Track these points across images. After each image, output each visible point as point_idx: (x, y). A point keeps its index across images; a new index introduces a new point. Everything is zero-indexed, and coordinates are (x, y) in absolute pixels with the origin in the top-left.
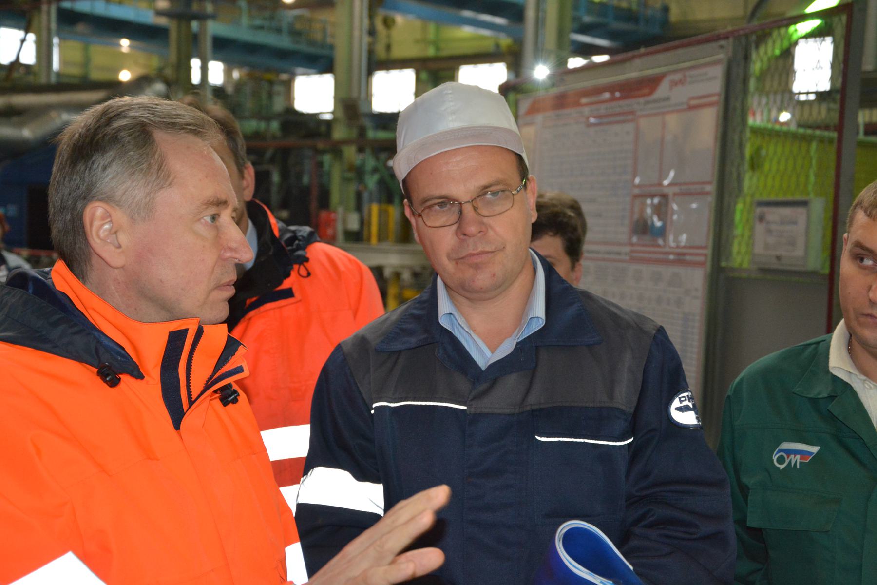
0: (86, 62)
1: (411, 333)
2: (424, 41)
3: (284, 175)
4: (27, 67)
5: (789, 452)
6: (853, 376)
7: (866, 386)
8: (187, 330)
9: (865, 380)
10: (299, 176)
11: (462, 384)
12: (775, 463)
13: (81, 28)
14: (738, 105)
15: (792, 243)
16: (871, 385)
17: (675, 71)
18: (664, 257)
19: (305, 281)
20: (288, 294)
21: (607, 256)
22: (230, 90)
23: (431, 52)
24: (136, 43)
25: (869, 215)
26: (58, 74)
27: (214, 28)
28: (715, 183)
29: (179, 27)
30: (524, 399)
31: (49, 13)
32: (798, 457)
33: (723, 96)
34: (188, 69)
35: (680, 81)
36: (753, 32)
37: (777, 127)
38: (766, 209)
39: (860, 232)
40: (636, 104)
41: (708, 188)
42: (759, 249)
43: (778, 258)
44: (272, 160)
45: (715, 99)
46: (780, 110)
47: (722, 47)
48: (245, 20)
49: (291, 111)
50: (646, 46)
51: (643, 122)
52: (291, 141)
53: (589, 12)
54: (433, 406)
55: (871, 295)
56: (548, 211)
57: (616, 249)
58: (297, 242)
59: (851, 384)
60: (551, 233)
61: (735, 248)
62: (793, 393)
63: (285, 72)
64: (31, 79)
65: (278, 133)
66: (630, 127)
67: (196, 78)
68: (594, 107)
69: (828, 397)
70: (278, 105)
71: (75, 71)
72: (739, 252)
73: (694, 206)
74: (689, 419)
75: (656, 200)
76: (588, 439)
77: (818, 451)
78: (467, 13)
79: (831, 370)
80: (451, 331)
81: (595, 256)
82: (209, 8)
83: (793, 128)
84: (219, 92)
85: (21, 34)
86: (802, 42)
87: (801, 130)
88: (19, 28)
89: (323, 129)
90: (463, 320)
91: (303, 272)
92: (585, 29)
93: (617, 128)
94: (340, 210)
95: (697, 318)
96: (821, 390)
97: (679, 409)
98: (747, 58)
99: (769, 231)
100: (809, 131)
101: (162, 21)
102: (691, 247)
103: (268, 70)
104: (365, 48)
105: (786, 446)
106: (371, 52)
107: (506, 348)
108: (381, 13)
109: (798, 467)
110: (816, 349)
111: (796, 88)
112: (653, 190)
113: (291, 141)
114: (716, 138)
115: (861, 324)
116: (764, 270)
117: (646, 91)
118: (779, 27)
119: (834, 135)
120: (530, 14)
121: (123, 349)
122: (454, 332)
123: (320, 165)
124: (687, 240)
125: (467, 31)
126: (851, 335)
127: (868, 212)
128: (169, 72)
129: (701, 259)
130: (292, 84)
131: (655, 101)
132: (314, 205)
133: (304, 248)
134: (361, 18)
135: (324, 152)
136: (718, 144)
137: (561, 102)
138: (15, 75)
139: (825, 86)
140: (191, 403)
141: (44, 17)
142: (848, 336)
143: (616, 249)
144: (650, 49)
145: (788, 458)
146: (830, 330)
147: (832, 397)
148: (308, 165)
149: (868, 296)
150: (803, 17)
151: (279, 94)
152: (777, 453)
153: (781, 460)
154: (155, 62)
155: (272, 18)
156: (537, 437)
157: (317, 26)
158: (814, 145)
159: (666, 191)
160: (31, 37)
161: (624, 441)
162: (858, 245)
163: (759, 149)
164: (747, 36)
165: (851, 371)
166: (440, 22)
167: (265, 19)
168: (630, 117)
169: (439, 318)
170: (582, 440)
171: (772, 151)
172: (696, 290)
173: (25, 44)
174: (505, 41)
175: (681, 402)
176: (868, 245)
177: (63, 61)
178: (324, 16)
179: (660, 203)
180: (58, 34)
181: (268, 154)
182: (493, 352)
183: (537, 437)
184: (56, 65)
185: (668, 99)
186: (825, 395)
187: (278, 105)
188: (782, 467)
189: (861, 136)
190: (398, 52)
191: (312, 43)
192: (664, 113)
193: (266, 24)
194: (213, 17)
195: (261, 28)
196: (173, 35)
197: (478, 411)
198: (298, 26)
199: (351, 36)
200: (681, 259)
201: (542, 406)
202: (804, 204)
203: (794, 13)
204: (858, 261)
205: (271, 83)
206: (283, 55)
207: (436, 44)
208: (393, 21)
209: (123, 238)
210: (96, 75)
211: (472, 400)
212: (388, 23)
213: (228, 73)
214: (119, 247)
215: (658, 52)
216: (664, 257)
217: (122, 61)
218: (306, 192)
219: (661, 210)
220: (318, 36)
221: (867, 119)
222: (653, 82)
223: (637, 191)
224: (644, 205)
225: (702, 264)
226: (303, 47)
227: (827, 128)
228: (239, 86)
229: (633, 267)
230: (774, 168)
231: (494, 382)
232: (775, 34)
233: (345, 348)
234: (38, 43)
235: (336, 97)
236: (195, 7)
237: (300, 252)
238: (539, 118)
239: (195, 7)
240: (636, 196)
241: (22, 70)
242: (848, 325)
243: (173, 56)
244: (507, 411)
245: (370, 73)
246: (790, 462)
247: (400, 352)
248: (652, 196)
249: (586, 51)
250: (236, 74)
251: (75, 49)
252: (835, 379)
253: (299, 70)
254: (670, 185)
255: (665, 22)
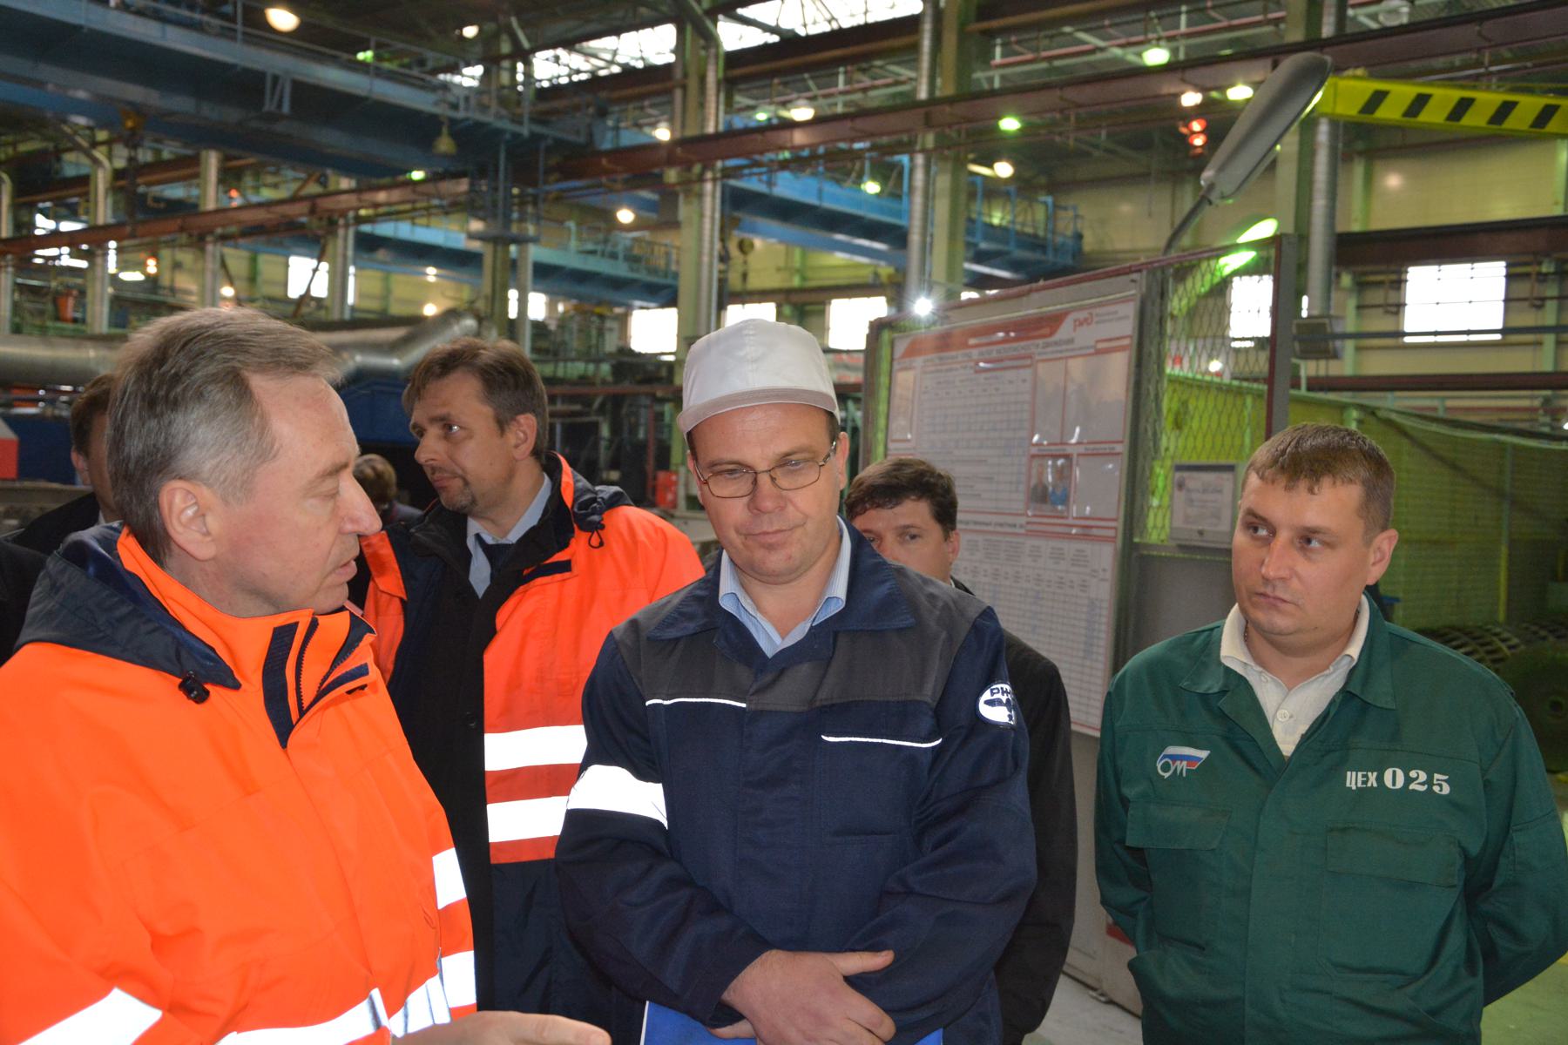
0: (386, 295)
1: (691, 617)
2: (787, 269)
3: (616, 429)
4: (319, 300)
5: (1174, 758)
6: (1249, 668)
7: (1263, 678)
8: (296, 624)
9: (1261, 672)
10: (633, 430)
11: (743, 674)
12: (1160, 771)
13: (381, 254)
14: (1154, 351)
15: (1217, 516)
16: (1269, 679)
17: (1081, 308)
18: (1066, 530)
19: (596, 553)
20: (565, 567)
21: (999, 529)
22: (553, 326)
23: (796, 282)
24: (442, 272)
25: (1262, 478)
26: (353, 309)
27: (536, 253)
28: (1127, 440)
29: (495, 252)
30: (816, 694)
31: (345, 239)
32: (1185, 763)
33: (1135, 341)
34: (505, 300)
35: (1086, 320)
36: (1170, 265)
37: (1208, 378)
38: (1186, 474)
39: (1252, 497)
40: (1035, 346)
41: (1119, 448)
42: (1178, 523)
43: (1201, 533)
44: (601, 410)
45: (1126, 342)
46: (1210, 358)
47: (1133, 281)
48: (573, 244)
49: (626, 351)
50: (1045, 279)
51: (1042, 368)
52: (626, 386)
53: (986, 238)
54: (710, 703)
55: (1264, 570)
56: (910, 471)
57: (1010, 519)
58: (595, 505)
59: (1246, 676)
60: (913, 497)
61: (1150, 522)
62: (1181, 688)
63: (619, 305)
64: (322, 314)
65: (610, 378)
66: (1026, 373)
67: (513, 313)
68: (984, 349)
69: (1219, 692)
70: (611, 344)
71: (374, 305)
72: (1155, 527)
73: (1110, 466)
74: (998, 715)
75: (1060, 462)
76: (887, 739)
77: (1208, 757)
78: (840, 237)
79: (1223, 661)
80: (734, 614)
81: (985, 528)
82: (531, 230)
83: (1226, 380)
84: (539, 327)
85: (314, 262)
86: (1236, 280)
87: (1236, 383)
88: (312, 257)
89: (664, 373)
90: (749, 601)
91: (595, 541)
92: (980, 257)
93: (1010, 374)
94: (682, 470)
95: (1105, 605)
96: (1212, 685)
97: (988, 703)
98: (1163, 295)
99: (1190, 501)
100: (1245, 384)
101: (476, 246)
102: (1093, 519)
103: (599, 303)
104: (716, 276)
105: (1172, 750)
106: (722, 282)
107: (798, 633)
108: (736, 236)
109: (1184, 775)
110: (1209, 636)
111: (1233, 333)
112: (1055, 450)
113: (626, 386)
114: (1127, 390)
115: (1254, 605)
116: (1182, 548)
117: (1046, 331)
118: (1209, 259)
119: (1264, 387)
120: (915, 238)
121: (213, 650)
122: (740, 616)
123: (659, 416)
124: (1090, 512)
125: (840, 257)
126: (1247, 622)
127: (1261, 473)
128: (481, 305)
129: (1111, 533)
130: (629, 319)
131: (1056, 343)
132: (650, 465)
133: (601, 513)
134: (712, 242)
135: (662, 401)
136: (1131, 394)
137: (945, 342)
138: (305, 310)
139: (1265, 331)
140: (302, 712)
141: (340, 242)
142: (1244, 622)
143: (1010, 519)
144: (1050, 282)
145: (1174, 764)
146: (1225, 616)
147: (1223, 692)
148: (644, 416)
149: (1260, 572)
150: (1235, 247)
151: (611, 330)
152: (1161, 760)
153: (1166, 768)
154: (466, 294)
155: (606, 241)
156: (823, 737)
157: (659, 251)
158: (1249, 400)
159: (1069, 450)
160: (324, 266)
161: (931, 742)
162: (1251, 513)
163: (1185, 404)
164: (1163, 269)
165: (1249, 663)
166: (806, 248)
167: (597, 243)
168: (1028, 362)
169: (720, 598)
170: (880, 741)
171: (1199, 405)
172: (1104, 570)
173: (317, 273)
174: (885, 270)
175: (992, 694)
176: (1261, 512)
177: (360, 294)
178: (667, 238)
179: (1062, 466)
180: (355, 264)
181: (596, 404)
182: (783, 638)
183: (823, 737)
184: (351, 300)
185: (1071, 341)
186: (1216, 690)
187: (611, 344)
188: (1166, 775)
189: (1303, 392)
190: (755, 283)
191: (653, 271)
192: (1067, 358)
193: (599, 248)
194: (535, 240)
195: (593, 252)
196: (488, 261)
197: (759, 708)
198: (636, 251)
199: (699, 264)
200: (1086, 534)
201: (834, 701)
202: (1230, 468)
203: (1227, 243)
204: (1251, 531)
205: (602, 317)
206: (617, 284)
207: (801, 272)
208: (752, 245)
209: (213, 522)
210: (396, 310)
211: (753, 694)
212: (744, 247)
213: (551, 306)
214: (208, 533)
215: (1060, 285)
216: (1066, 530)
217: (427, 291)
218: (641, 447)
219: (1063, 474)
220: (662, 263)
221: (1312, 373)
222: (1054, 321)
223: (1034, 451)
224: (1043, 467)
225: (1112, 539)
226: (643, 276)
227: (1256, 380)
228: (563, 322)
229: (1031, 542)
230: (1205, 426)
231: (782, 672)
232: (1204, 265)
233: (617, 636)
234: (332, 273)
235: (678, 336)
236: (514, 229)
237: (595, 518)
238: (919, 361)
239: (514, 229)
240: (1033, 456)
241: (313, 304)
242: (1243, 610)
243: (486, 288)
244: (795, 709)
245: (721, 307)
246: (1176, 769)
247: (677, 640)
248: (1055, 457)
249: (980, 282)
250: (561, 308)
251: (374, 280)
252: (1228, 671)
253: (638, 303)
254: (1079, 443)
255: (1078, 252)
